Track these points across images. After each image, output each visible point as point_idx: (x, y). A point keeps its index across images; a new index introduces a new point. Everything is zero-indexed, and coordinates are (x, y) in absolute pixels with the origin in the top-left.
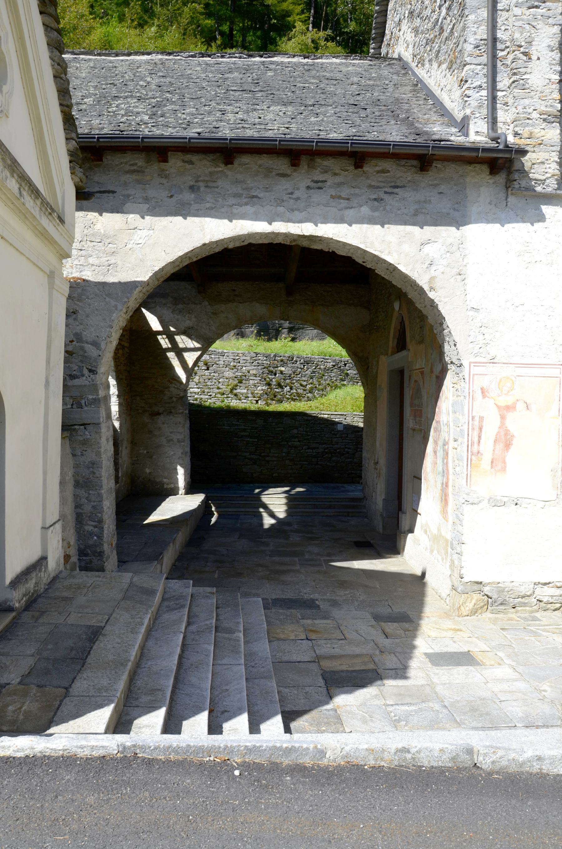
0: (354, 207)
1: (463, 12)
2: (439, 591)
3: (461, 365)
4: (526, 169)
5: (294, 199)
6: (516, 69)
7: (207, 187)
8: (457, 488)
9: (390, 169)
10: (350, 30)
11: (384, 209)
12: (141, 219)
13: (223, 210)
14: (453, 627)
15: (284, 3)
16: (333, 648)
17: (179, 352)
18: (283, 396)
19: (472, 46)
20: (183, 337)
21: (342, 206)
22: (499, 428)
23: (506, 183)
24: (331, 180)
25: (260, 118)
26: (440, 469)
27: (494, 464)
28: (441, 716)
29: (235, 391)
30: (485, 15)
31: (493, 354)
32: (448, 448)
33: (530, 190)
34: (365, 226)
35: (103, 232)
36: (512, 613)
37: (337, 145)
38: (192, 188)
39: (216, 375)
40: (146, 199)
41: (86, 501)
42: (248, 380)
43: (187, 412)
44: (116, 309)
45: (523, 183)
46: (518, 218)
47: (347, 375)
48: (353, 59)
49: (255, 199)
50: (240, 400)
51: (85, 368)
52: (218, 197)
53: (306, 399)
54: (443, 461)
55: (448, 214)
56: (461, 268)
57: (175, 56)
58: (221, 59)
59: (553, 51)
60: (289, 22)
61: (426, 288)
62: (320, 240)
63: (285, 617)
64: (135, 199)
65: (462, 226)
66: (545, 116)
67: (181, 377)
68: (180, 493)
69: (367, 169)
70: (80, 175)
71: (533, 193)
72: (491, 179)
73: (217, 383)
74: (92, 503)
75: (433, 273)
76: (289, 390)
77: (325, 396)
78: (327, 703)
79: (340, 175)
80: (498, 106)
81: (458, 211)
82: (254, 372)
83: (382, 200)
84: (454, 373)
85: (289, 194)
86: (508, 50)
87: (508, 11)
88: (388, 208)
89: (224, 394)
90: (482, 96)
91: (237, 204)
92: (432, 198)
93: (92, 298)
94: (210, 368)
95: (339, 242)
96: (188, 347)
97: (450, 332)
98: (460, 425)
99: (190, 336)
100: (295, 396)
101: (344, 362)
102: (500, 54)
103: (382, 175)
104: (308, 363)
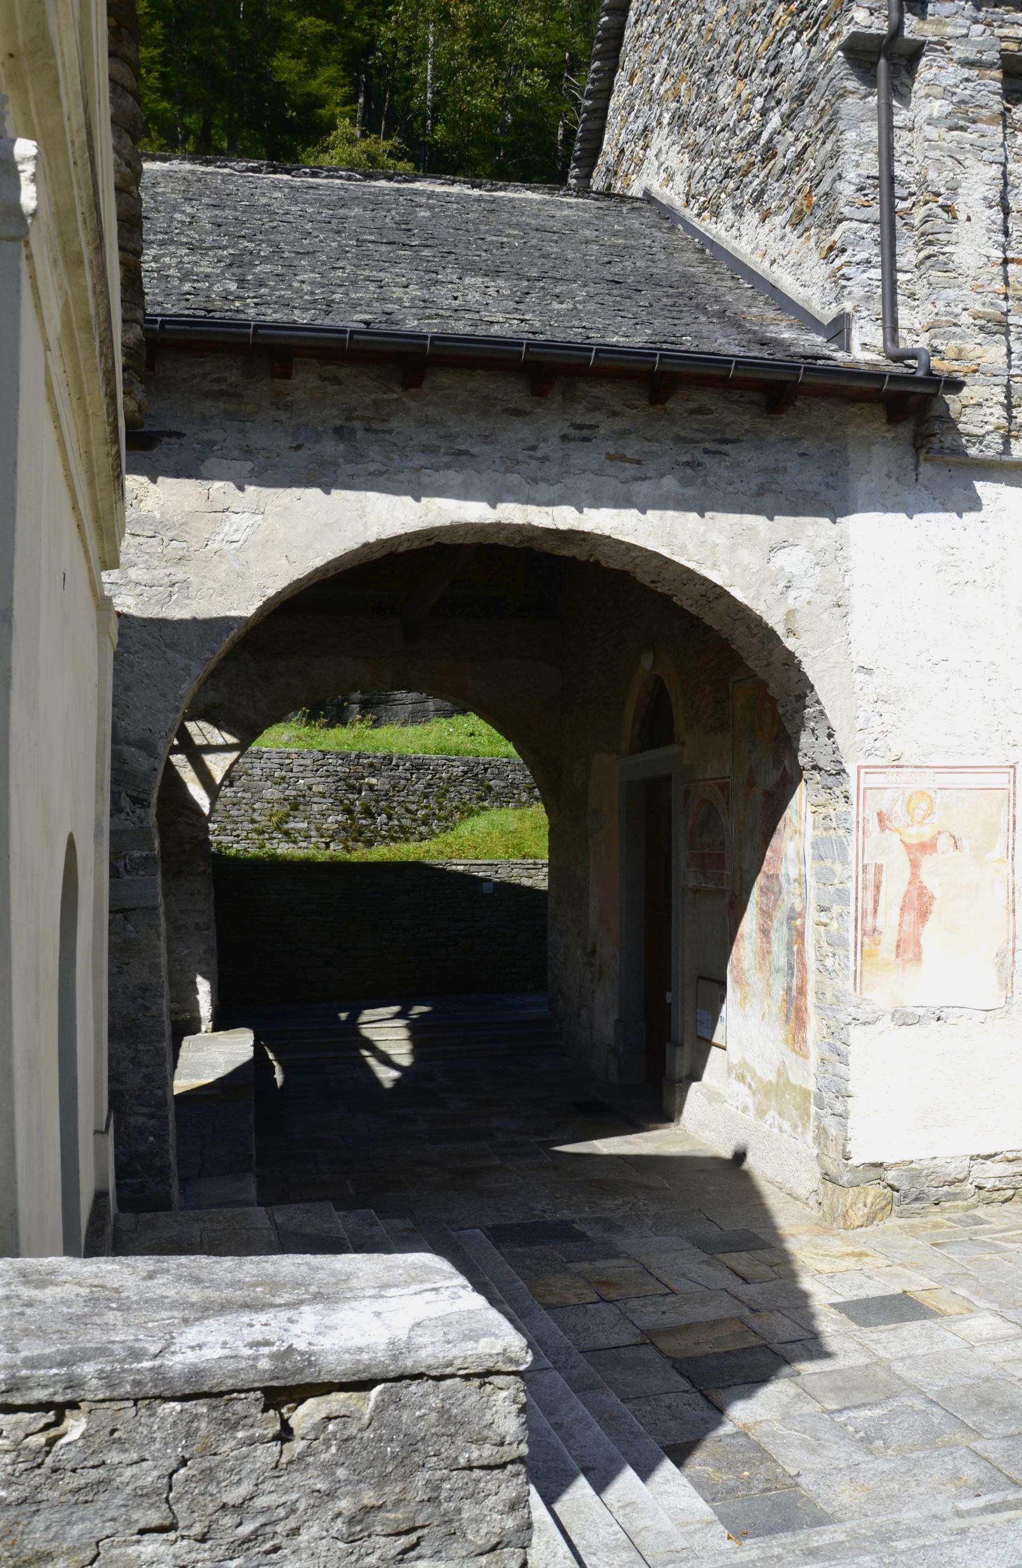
0: (650, 478)
1: (832, 124)
2: (788, 1185)
3: (841, 772)
4: (953, 415)
5: (537, 459)
6: (932, 234)
7: (368, 430)
8: (829, 995)
9: (713, 408)
10: (435, 141)
11: (704, 483)
12: (237, 491)
13: (402, 477)
14: (850, 1250)
15: (311, 81)
16: (664, 1313)
17: (195, 754)
18: (376, 832)
19: (854, 188)
20: (203, 724)
21: (629, 474)
22: (910, 883)
23: (915, 439)
24: (607, 425)
25: (456, 298)
26: (783, 962)
27: (901, 950)
28: (936, 1421)
29: (286, 826)
30: (874, 133)
31: (896, 751)
32: (804, 924)
33: (958, 454)
34: (670, 513)
35: (158, 515)
36: (935, 1214)
37: (615, 356)
38: (339, 432)
39: (248, 795)
40: (247, 452)
41: (131, 1066)
42: (309, 803)
43: (210, 870)
44: (189, 675)
45: (948, 441)
46: (937, 504)
47: (490, 788)
48: (565, 195)
49: (463, 458)
50: (295, 842)
51: (123, 794)
52: (392, 452)
53: (417, 836)
54: (789, 948)
55: (817, 494)
56: (840, 594)
57: (219, 167)
58: (310, 180)
59: (991, 207)
60: (320, 117)
61: (780, 631)
62: (583, 540)
63: (534, 1261)
64: (224, 451)
65: (842, 516)
66: (983, 322)
67: (200, 802)
68: (203, 1028)
69: (671, 406)
70: (140, 396)
71: (962, 459)
72: (888, 431)
73: (250, 811)
74: (143, 1070)
76: (386, 821)
77: (452, 830)
78: (719, 1423)
79: (623, 415)
80: (900, 298)
81: (834, 489)
82: (321, 788)
83: (699, 464)
84: (820, 786)
85: (529, 449)
86: (914, 198)
87: (911, 130)
88: (711, 479)
89: (262, 832)
90: (871, 279)
91: (429, 465)
92: (789, 464)
93: (137, 652)
94: (237, 783)
95: (623, 542)
96: (213, 742)
97: (822, 712)
98: (836, 881)
99: (216, 723)
100: (396, 832)
101: (484, 764)
102: (901, 205)
103: (700, 417)
104: (419, 769)
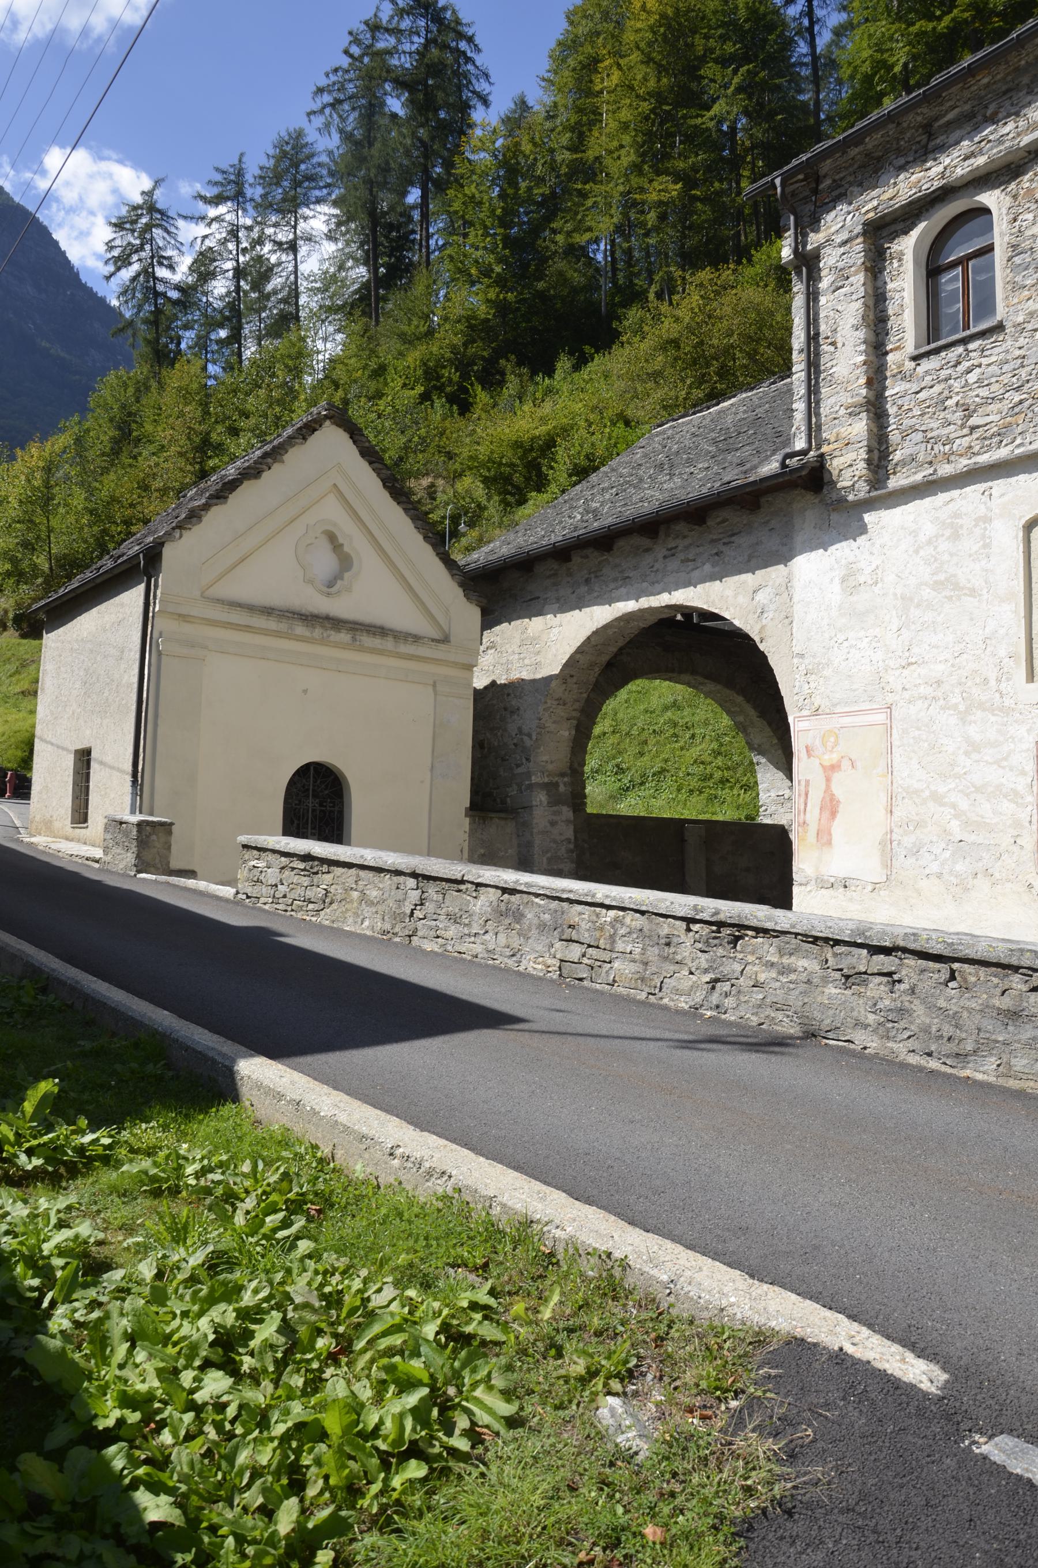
24: (682, 543)
61: (757, 639)
75: (764, 622)
